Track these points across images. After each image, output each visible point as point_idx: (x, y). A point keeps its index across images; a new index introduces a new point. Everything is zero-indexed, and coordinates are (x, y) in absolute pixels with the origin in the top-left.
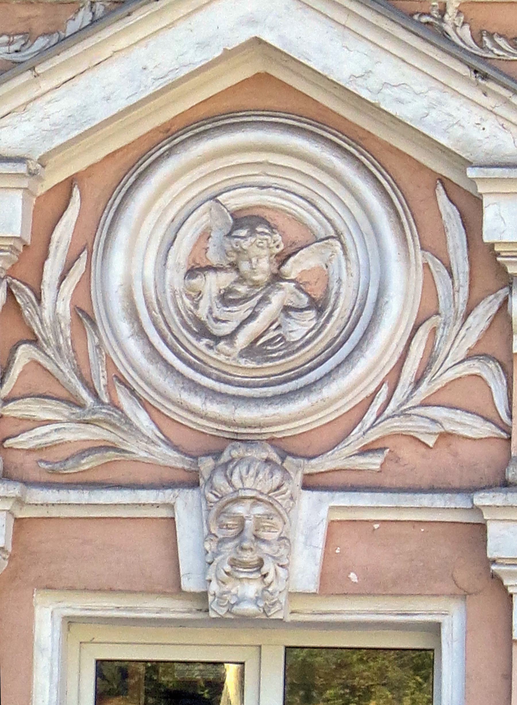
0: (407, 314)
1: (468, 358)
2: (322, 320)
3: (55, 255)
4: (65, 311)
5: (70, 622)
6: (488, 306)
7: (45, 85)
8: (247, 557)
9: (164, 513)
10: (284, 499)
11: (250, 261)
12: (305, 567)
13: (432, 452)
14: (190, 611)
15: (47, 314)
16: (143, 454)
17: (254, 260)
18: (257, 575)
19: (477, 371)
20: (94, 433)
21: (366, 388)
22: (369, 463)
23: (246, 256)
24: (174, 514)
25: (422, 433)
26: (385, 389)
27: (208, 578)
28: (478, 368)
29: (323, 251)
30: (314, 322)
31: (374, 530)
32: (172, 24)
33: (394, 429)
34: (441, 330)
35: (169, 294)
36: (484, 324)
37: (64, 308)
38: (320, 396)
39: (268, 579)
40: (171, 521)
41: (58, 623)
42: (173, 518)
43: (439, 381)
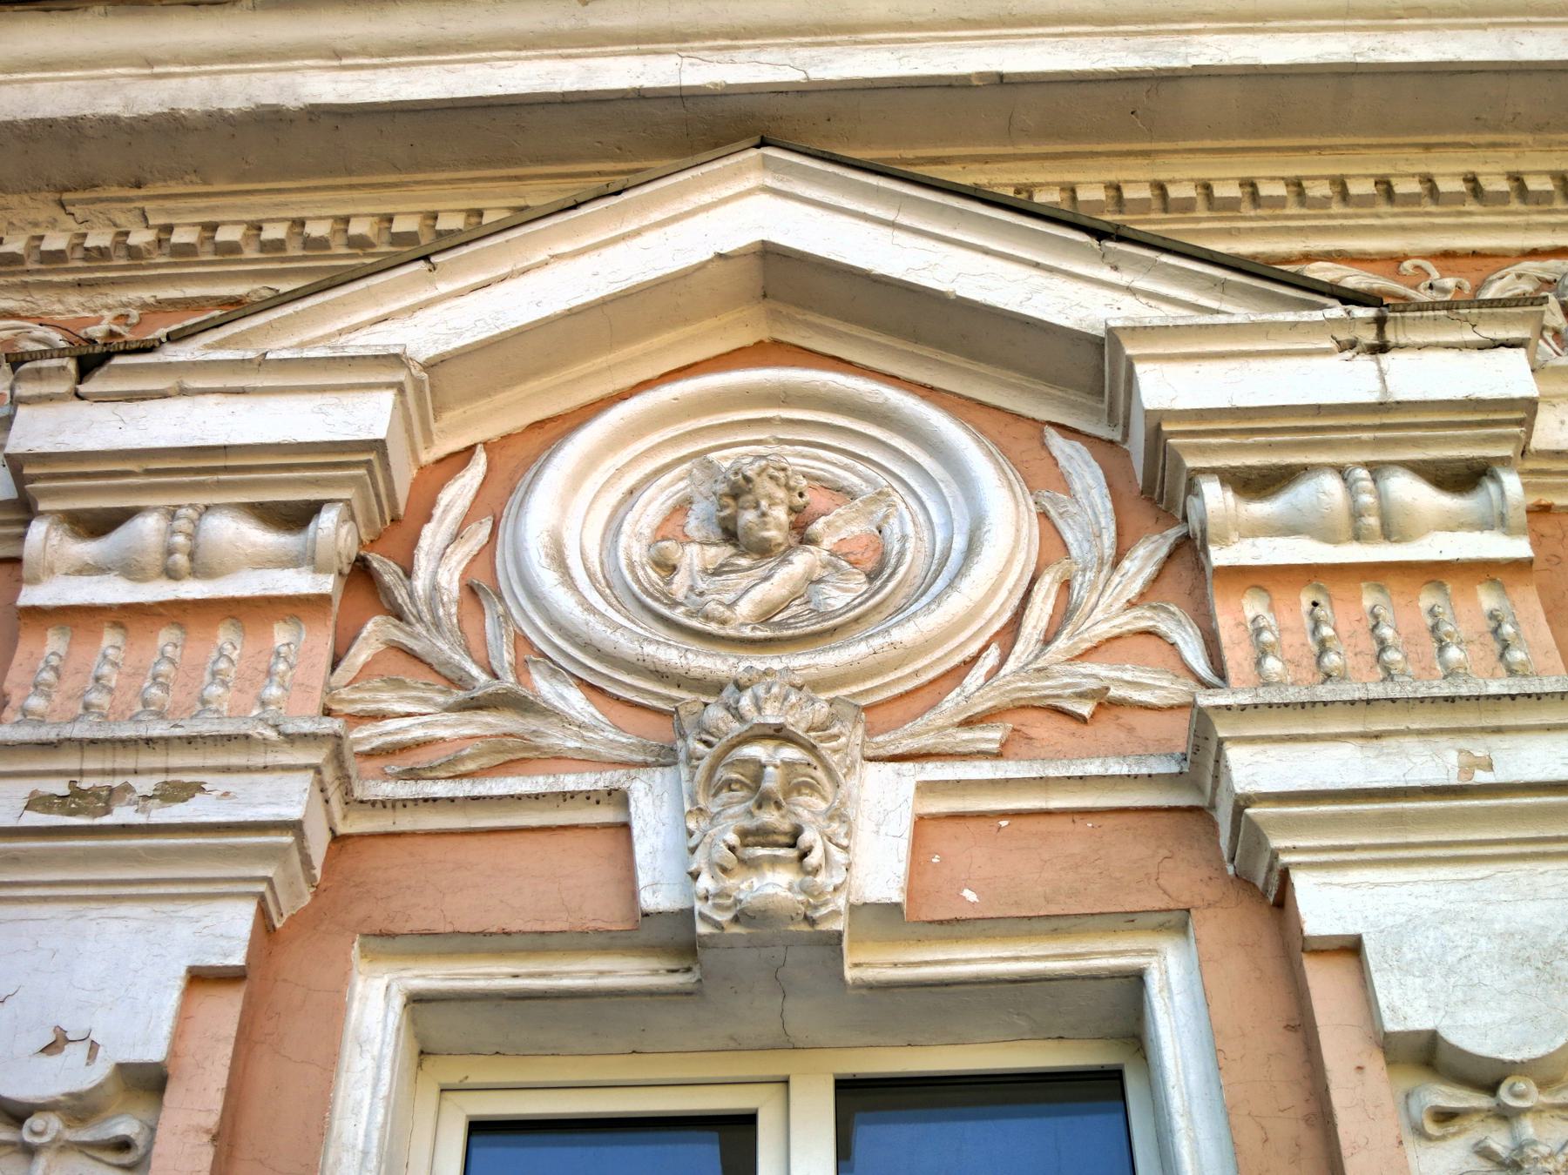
0: (1021, 557)
1: (1131, 604)
2: (878, 583)
3: (441, 521)
4: (450, 582)
5: (416, 1000)
6: (1152, 547)
7: (444, 288)
8: (770, 817)
9: (606, 815)
10: (835, 751)
11: (757, 506)
12: (876, 866)
13: (1087, 730)
14: (655, 972)
15: (421, 583)
16: (572, 744)
17: (764, 503)
18: (792, 853)
19: (1143, 624)
20: (488, 724)
21: (963, 645)
22: (978, 740)
23: (750, 497)
24: (629, 814)
25: (1069, 697)
26: (993, 654)
27: (693, 867)
28: (1151, 619)
29: (873, 508)
30: (865, 587)
31: (1000, 828)
32: (637, 233)
33: (1020, 695)
34: (1080, 579)
35: (623, 563)
36: (1150, 570)
37: (450, 581)
38: (888, 639)
39: (814, 859)
40: (624, 830)
41: (398, 1002)
42: (626, 827)
43: (1086, 635)
